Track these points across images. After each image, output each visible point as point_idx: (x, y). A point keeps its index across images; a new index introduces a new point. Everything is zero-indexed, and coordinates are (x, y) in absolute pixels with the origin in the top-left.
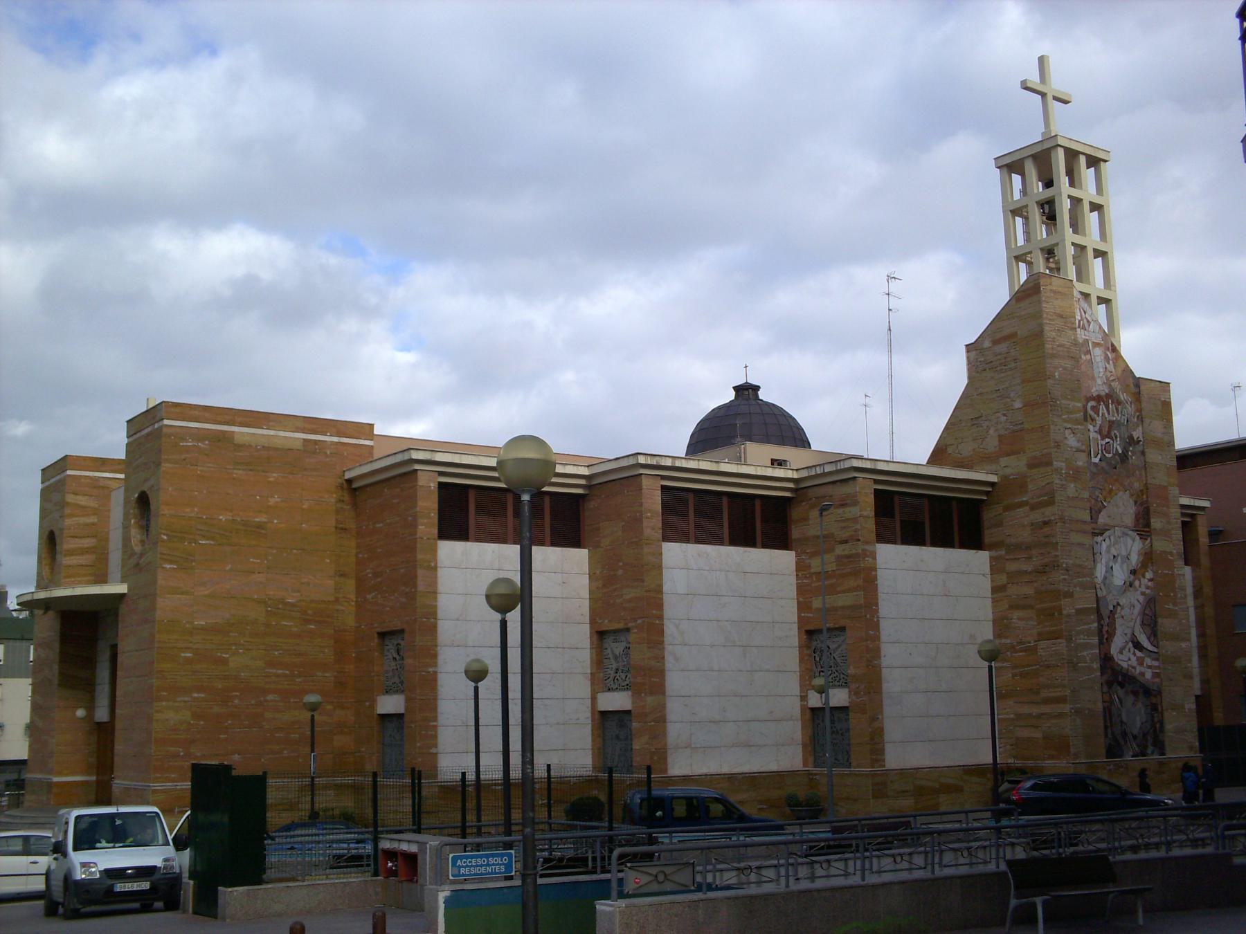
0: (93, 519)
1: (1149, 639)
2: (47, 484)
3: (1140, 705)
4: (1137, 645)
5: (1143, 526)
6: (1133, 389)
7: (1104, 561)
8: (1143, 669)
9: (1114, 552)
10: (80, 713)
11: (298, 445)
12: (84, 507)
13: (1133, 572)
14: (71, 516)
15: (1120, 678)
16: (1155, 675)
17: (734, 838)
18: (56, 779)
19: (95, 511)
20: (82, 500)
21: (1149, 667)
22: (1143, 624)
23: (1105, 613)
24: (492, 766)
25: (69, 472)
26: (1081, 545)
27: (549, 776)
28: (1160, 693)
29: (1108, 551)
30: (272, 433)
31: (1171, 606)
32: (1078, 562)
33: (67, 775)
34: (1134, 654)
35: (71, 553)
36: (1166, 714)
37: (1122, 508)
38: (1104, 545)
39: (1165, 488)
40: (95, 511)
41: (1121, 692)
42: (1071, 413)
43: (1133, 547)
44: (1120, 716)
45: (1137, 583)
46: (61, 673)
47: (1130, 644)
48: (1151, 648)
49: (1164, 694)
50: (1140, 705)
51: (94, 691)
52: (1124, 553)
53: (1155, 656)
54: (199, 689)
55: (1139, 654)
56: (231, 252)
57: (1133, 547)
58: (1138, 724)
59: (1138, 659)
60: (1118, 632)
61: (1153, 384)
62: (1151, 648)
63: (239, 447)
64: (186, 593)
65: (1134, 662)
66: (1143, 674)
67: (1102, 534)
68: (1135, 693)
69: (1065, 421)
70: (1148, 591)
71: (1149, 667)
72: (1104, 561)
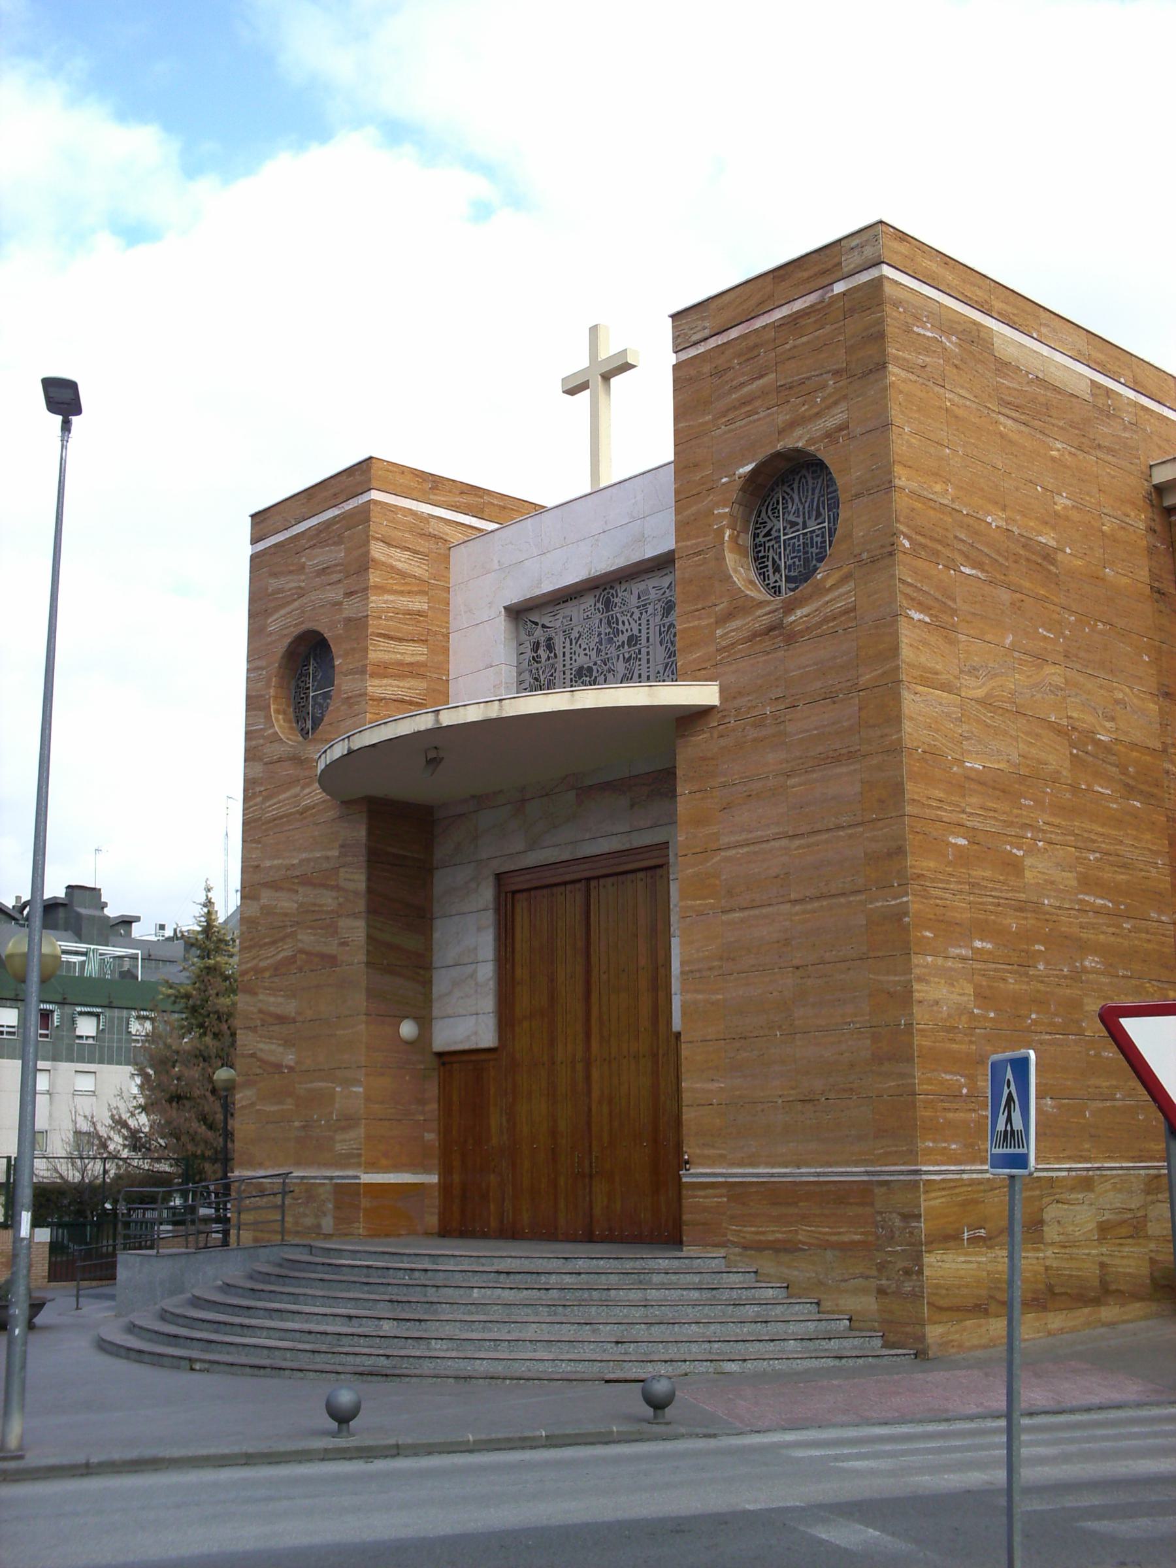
0: (419, 604)
2: (261, 546)
10: (408, 1029)
11: (1083, 390)
12: (403, 574)
14: (382, 589)
17: (670, 1369)
18: (366, 1178)
19: (422, 587)
20: (400, 560)
25: (375, 495)
27: (78, 1297)
30: (1045, 350)
33: (386, 1170)
35: (384, 670)
40: (422, 587)
46: (370, 938)
51: (428, 983)
54: (983, 929)
63: (1003, 366)
64: (946, 687)
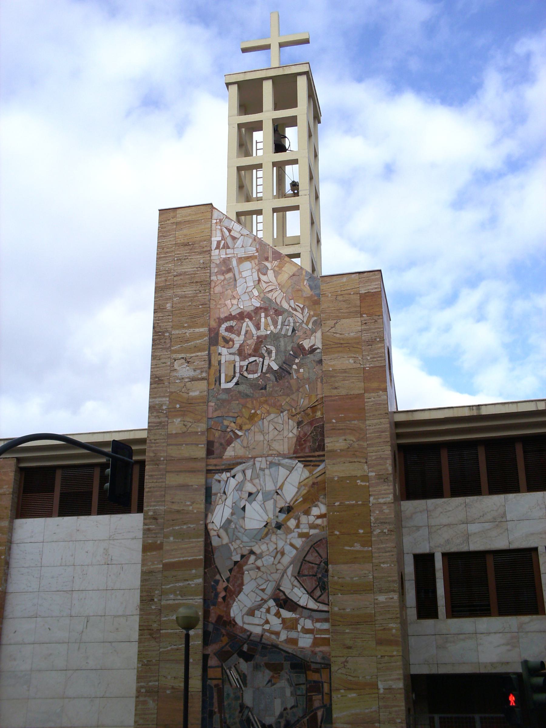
1: (311, 594)
3: (283, 683)
4: (285, 602)
5: (310, 448)
6: (307, 291)
7: (229, 502)
8: (293, 635)
9: (249, 487)
13: (288, 510)
15: (245, 648)
16: (316, 642)
21: (306, 631)
22: (299, 575)
23: (223, 564)
24: (366, 400)
26: (184, 487)
28: (328, 666)
29: (240, 487)
31: (357, 547)
32: (175, 507)
34: (278, 615)
36: (335, 696)
37: (279, 430)
38: (233, 482)
39: (360, 396)
41: (244, 666)
42: (187, 341)
43: (292, 480)
44: (239, 697)
45: (292, 523)
47: (271, 603)
48: (312, 605)
49: (334, 668)
50: (283, 683)
52: (270, 487)
53: (325, 616)
55: (286, 614)
56: (347, 631)
57: (292, 480)
58: (278, 710)
59: (284, 621)
60: (247, 588)
61: (344, 279)
62: (312, 605)
65: (275, 623)
66: (294, 641)
67: (228, 470)
68: (276, 668)
69: (176, 352)
70: (312, 532)
71: (306, 631)
72: (229, 502)
